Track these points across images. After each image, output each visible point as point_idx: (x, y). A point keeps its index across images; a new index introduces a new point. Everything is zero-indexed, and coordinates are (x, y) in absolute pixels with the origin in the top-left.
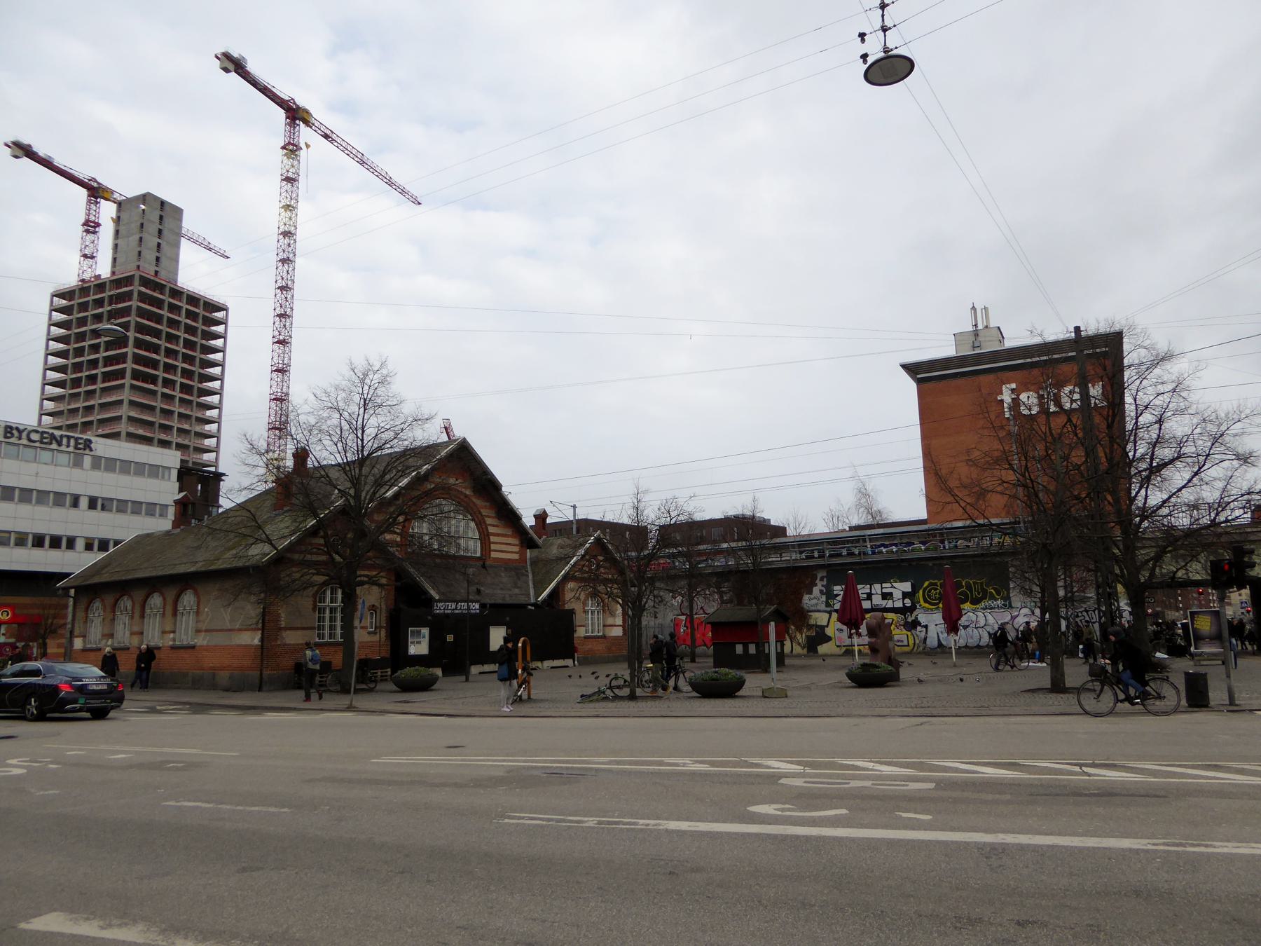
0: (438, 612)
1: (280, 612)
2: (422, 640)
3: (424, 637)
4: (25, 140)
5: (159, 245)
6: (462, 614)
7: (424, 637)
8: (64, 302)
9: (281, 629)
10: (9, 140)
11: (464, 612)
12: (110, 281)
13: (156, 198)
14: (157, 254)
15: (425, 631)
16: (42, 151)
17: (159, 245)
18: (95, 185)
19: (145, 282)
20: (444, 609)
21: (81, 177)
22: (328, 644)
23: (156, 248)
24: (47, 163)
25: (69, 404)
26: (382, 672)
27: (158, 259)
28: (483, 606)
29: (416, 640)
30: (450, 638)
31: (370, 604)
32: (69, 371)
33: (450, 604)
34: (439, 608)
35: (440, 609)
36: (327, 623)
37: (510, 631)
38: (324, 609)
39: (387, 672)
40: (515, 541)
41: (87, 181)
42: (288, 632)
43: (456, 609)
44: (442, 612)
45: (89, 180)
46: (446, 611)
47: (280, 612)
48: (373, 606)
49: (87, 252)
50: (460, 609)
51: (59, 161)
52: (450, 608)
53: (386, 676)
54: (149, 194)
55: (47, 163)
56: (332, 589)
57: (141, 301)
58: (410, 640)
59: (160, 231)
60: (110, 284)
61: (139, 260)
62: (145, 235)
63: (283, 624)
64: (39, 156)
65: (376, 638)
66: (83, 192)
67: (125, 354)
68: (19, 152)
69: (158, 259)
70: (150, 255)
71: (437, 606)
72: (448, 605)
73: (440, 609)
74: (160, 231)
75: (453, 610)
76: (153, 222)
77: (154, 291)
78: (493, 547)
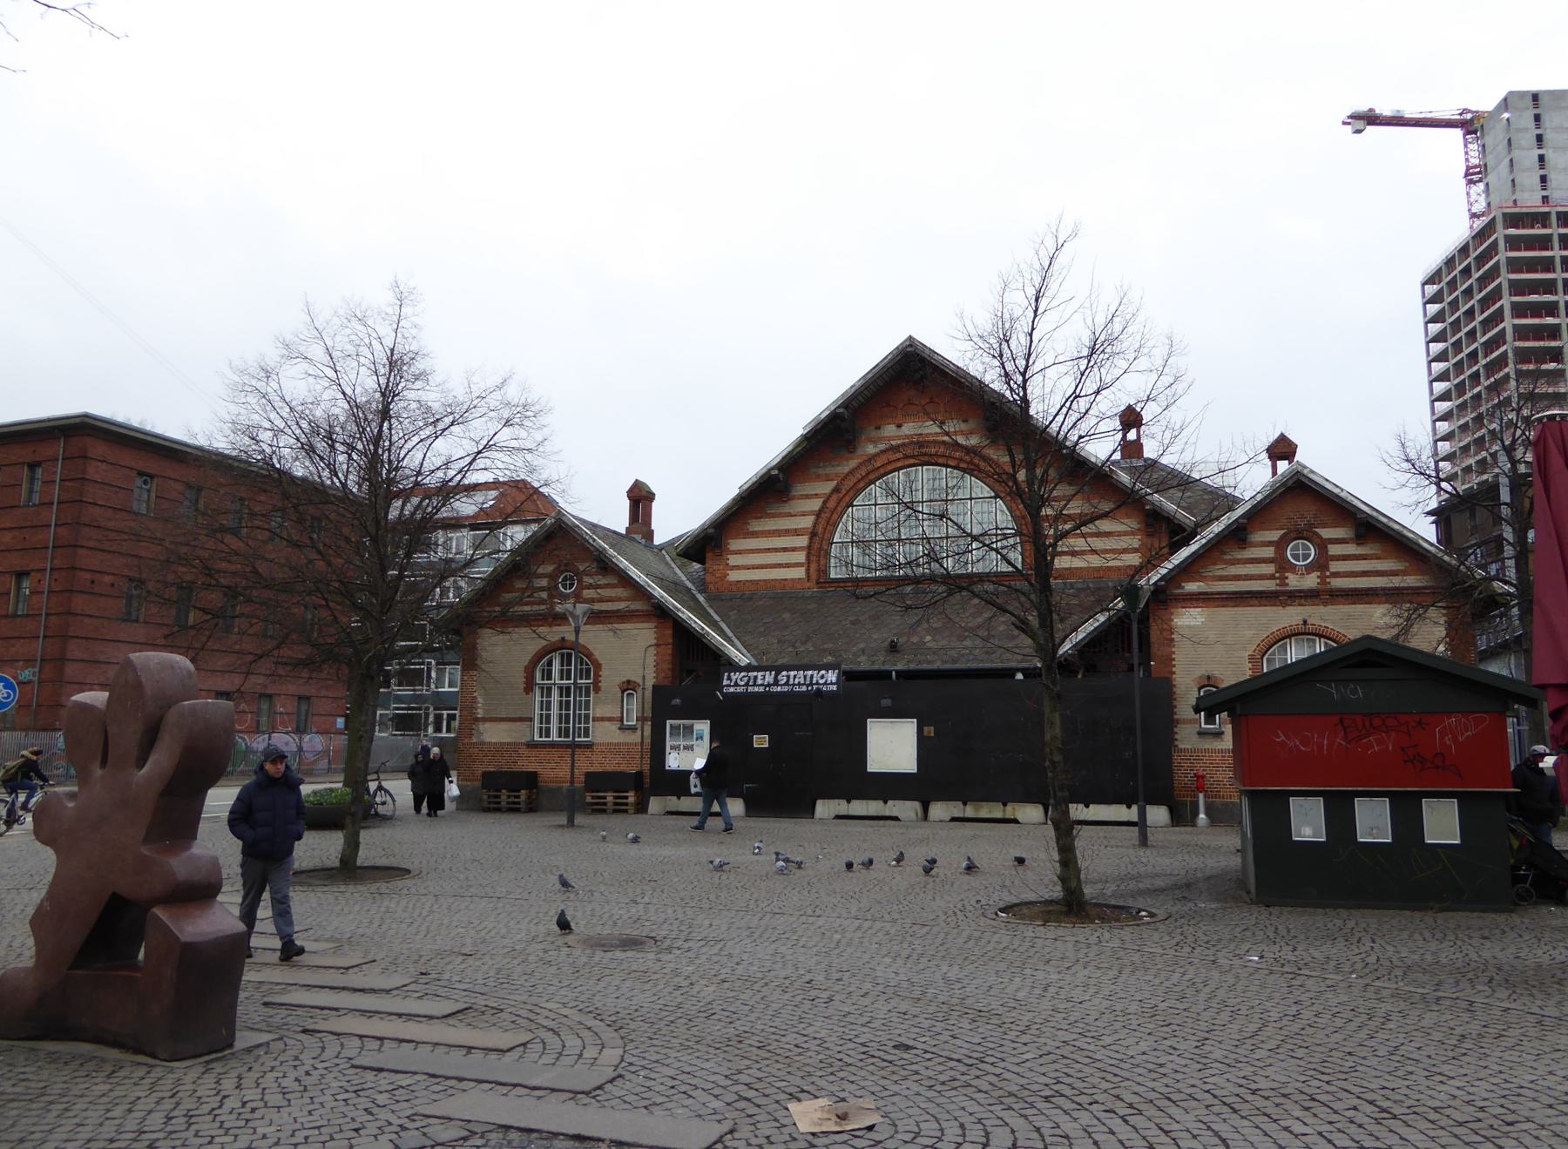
0: (732, 690)
1: (475, 694)
2: (695, 742)
3: (700, 737)
4: (1363, 107)
5: (1541, 158)
6: (791, 694)
7: (700, 737)
8: (1435, 288)
9: (477, 720)
10: (1344, 117)
11: (797, 689)
12: (1473, 238)
13: (1521, 95)
14: (1542, 172)
15: (703, 727)
16: (1385, 110)
17: (1541, 158)
18: (1469, 116)
19: (1514, 220)
20: (747, 684)
21: (1446, 115)
22: (553, 745)
23: (1537, 164)
24: (1398, 121)
25: (1458, 420)
26: (615, 798)
27: (1543, 179)
28: (849, 676)
29: (682, 743)
30: (761, 741)
31: (625, 679)
32: (1452, 378)
33: (760, 674)
34: (734, 683)
35: (736, 685)
36: (555, 711)
37: (929, 731)
38: (549, 689)
39: (627, 798)
40: (1132, 523)
41: (1458, 117)
42: (488, 725)
43: (776, 683)
44: (739, 690)
45: (1461, 114)
46: (750, 689)
47: (475, 694)
48: (629, 682)
49: (1474, 210)
50: (787, 684)
51: (1410, 112)
52: (759, 682)
53: (626, 804)
54: (1511, 93)
55: (1398, 121)
56: (562, 655)
57: (1512, 249)
58: (669, 743)
59: (1539, 138)
60: (1473, 242)
61: (1514, 192)
62: (1516, 154)
63: (480, 713)
64: (1386, 117)
65: (635, 738)
66: (1458, 133)
67: (1503, 331)
68: (1360, 124)
69: (1543, 179)
70: (1530, 179)
71: (729, 678)
72: (756, 677)
73: (736, 685)
74: (1539, 138)
75: (769, 685)
76: (1526, 130)
77: (1533, 227)
78: (801, 557)
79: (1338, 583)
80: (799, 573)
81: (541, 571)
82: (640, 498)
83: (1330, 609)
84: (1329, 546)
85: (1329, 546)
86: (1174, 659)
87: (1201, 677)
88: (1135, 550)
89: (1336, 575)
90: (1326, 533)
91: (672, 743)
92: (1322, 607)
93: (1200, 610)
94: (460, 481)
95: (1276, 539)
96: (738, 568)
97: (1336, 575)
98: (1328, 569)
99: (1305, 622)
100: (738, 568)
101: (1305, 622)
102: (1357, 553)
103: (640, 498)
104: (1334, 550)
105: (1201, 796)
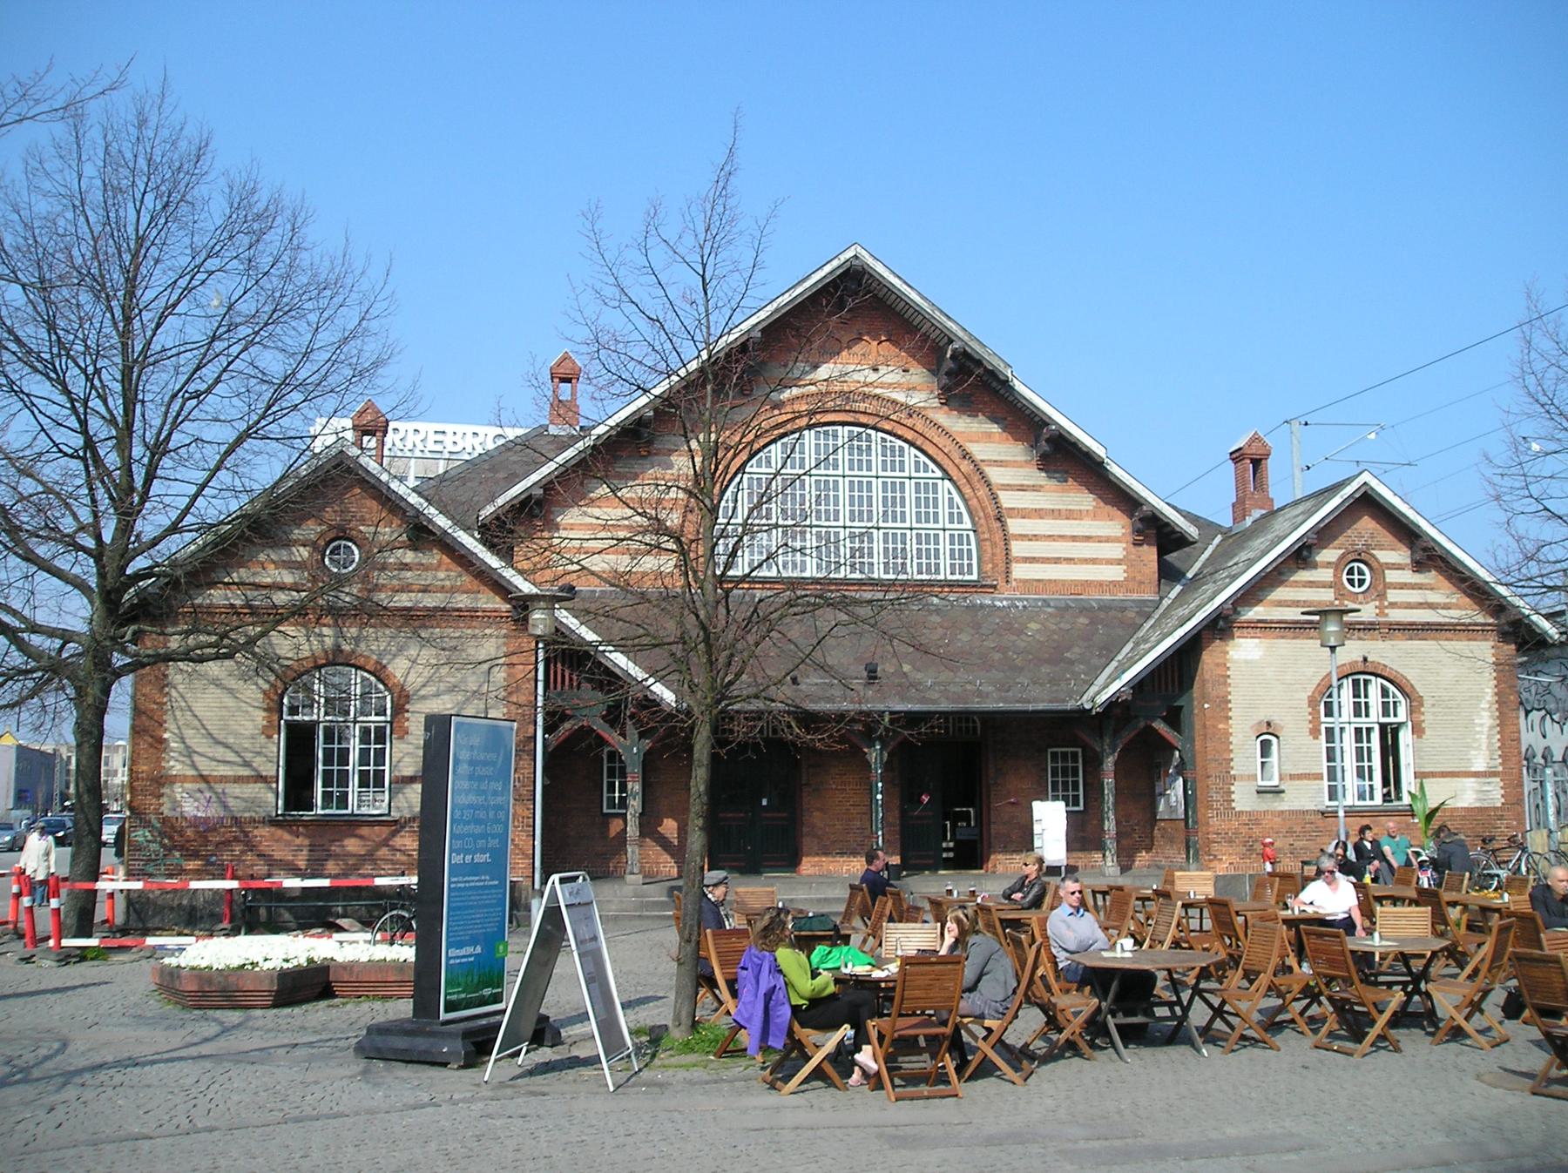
78: (1018, 548)
79: (1396, 615)
80: (1117, 573)
81: (297, 534)
82: (1251, 461)
83: (1388, 643)
84: (1387, 572)
85: (1387, 572)
86: (1230, 701)
87: (1260, 723)
88: (1119, 562)
89: (1393, 605)
90: (1384, 556)
91: (458, 859)
92: (1380, 642)
93: (1257, 640)
94: (6, 348)
95: (1334, 560)
96: (1109, 562)
97: (1393, 605)
98: (1386, 599)
99: (1365, 659)
100: (1109, 562)
101: (1365, 659)
102: (1413, 581)
103: (1251, 461)
104: (1392, 576)
105: (1467, 874)
